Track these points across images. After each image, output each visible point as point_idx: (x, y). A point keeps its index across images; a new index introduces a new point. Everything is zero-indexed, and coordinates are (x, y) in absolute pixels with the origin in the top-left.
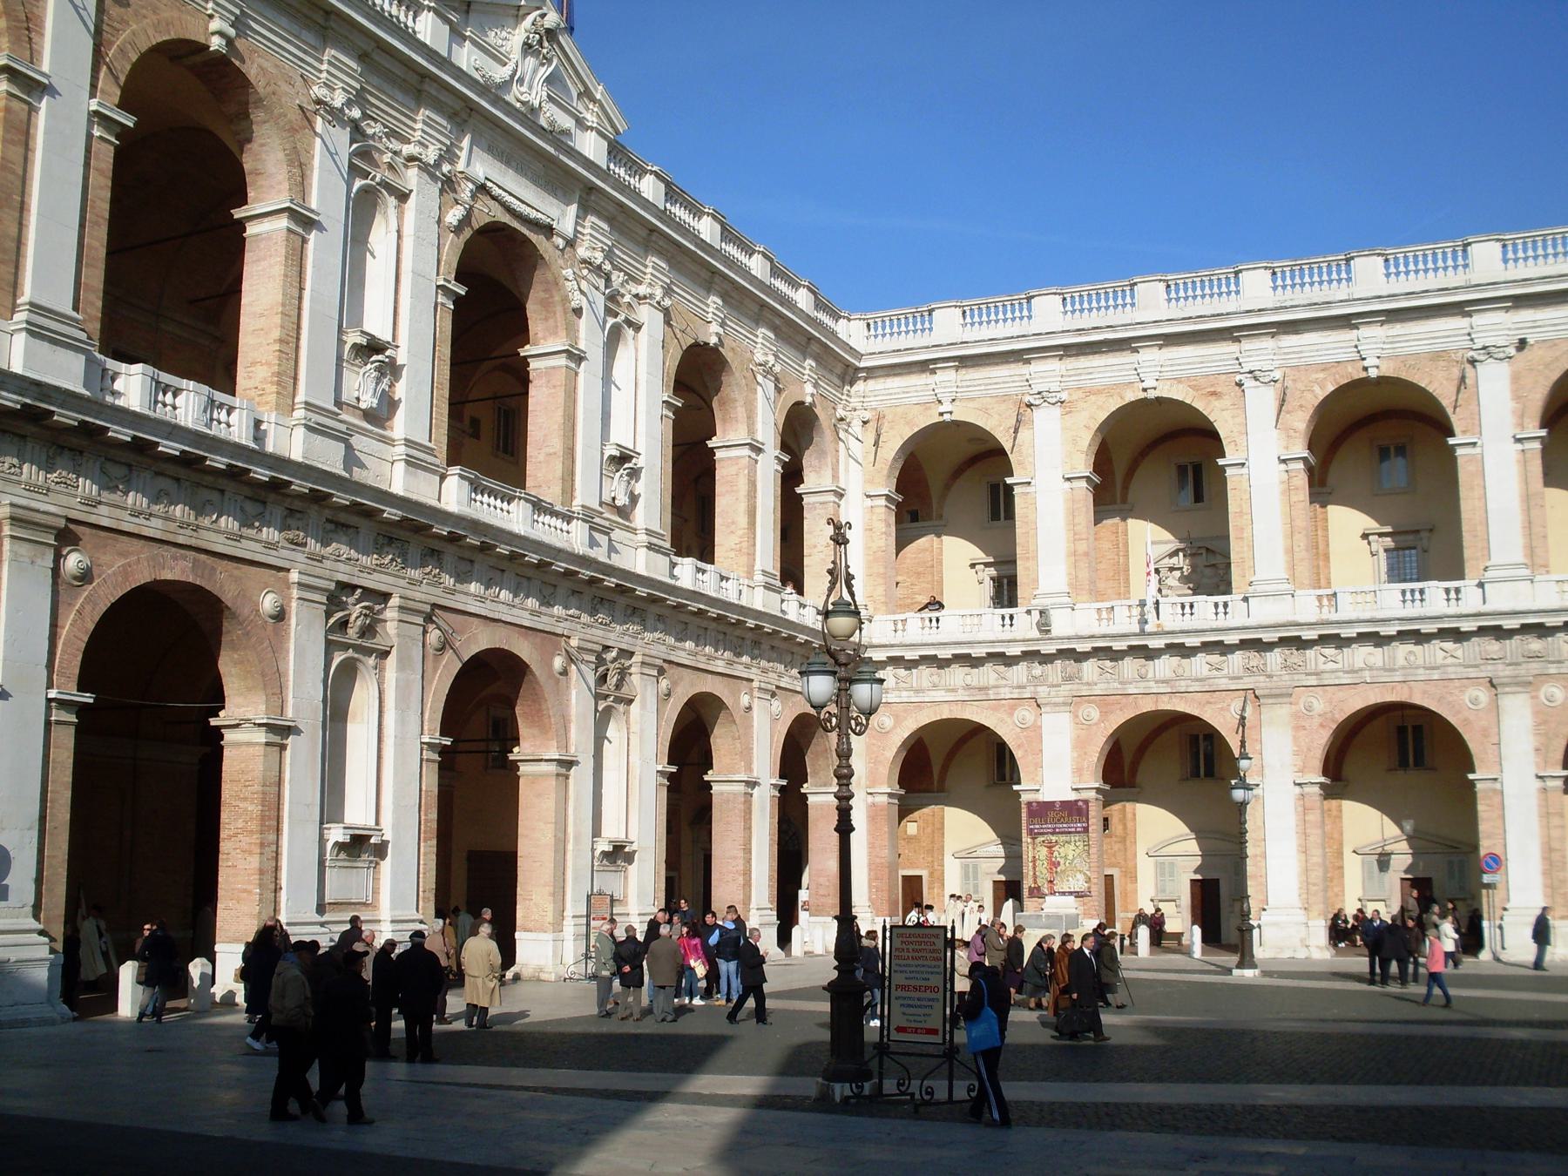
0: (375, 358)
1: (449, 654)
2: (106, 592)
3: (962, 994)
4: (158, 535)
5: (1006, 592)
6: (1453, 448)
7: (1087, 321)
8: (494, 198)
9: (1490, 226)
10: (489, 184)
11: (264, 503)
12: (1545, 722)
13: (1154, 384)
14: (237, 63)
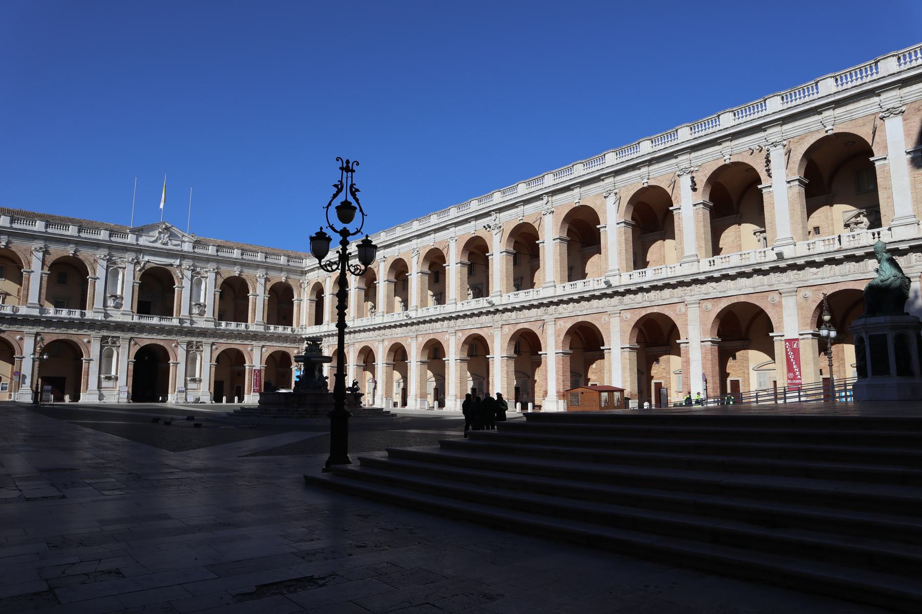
2: (138, 348)
5: (406, 307)
6: (761, 190)
7: (624, 159)
9: (680, 122)
12: (802, 309)
13: (831, 127)
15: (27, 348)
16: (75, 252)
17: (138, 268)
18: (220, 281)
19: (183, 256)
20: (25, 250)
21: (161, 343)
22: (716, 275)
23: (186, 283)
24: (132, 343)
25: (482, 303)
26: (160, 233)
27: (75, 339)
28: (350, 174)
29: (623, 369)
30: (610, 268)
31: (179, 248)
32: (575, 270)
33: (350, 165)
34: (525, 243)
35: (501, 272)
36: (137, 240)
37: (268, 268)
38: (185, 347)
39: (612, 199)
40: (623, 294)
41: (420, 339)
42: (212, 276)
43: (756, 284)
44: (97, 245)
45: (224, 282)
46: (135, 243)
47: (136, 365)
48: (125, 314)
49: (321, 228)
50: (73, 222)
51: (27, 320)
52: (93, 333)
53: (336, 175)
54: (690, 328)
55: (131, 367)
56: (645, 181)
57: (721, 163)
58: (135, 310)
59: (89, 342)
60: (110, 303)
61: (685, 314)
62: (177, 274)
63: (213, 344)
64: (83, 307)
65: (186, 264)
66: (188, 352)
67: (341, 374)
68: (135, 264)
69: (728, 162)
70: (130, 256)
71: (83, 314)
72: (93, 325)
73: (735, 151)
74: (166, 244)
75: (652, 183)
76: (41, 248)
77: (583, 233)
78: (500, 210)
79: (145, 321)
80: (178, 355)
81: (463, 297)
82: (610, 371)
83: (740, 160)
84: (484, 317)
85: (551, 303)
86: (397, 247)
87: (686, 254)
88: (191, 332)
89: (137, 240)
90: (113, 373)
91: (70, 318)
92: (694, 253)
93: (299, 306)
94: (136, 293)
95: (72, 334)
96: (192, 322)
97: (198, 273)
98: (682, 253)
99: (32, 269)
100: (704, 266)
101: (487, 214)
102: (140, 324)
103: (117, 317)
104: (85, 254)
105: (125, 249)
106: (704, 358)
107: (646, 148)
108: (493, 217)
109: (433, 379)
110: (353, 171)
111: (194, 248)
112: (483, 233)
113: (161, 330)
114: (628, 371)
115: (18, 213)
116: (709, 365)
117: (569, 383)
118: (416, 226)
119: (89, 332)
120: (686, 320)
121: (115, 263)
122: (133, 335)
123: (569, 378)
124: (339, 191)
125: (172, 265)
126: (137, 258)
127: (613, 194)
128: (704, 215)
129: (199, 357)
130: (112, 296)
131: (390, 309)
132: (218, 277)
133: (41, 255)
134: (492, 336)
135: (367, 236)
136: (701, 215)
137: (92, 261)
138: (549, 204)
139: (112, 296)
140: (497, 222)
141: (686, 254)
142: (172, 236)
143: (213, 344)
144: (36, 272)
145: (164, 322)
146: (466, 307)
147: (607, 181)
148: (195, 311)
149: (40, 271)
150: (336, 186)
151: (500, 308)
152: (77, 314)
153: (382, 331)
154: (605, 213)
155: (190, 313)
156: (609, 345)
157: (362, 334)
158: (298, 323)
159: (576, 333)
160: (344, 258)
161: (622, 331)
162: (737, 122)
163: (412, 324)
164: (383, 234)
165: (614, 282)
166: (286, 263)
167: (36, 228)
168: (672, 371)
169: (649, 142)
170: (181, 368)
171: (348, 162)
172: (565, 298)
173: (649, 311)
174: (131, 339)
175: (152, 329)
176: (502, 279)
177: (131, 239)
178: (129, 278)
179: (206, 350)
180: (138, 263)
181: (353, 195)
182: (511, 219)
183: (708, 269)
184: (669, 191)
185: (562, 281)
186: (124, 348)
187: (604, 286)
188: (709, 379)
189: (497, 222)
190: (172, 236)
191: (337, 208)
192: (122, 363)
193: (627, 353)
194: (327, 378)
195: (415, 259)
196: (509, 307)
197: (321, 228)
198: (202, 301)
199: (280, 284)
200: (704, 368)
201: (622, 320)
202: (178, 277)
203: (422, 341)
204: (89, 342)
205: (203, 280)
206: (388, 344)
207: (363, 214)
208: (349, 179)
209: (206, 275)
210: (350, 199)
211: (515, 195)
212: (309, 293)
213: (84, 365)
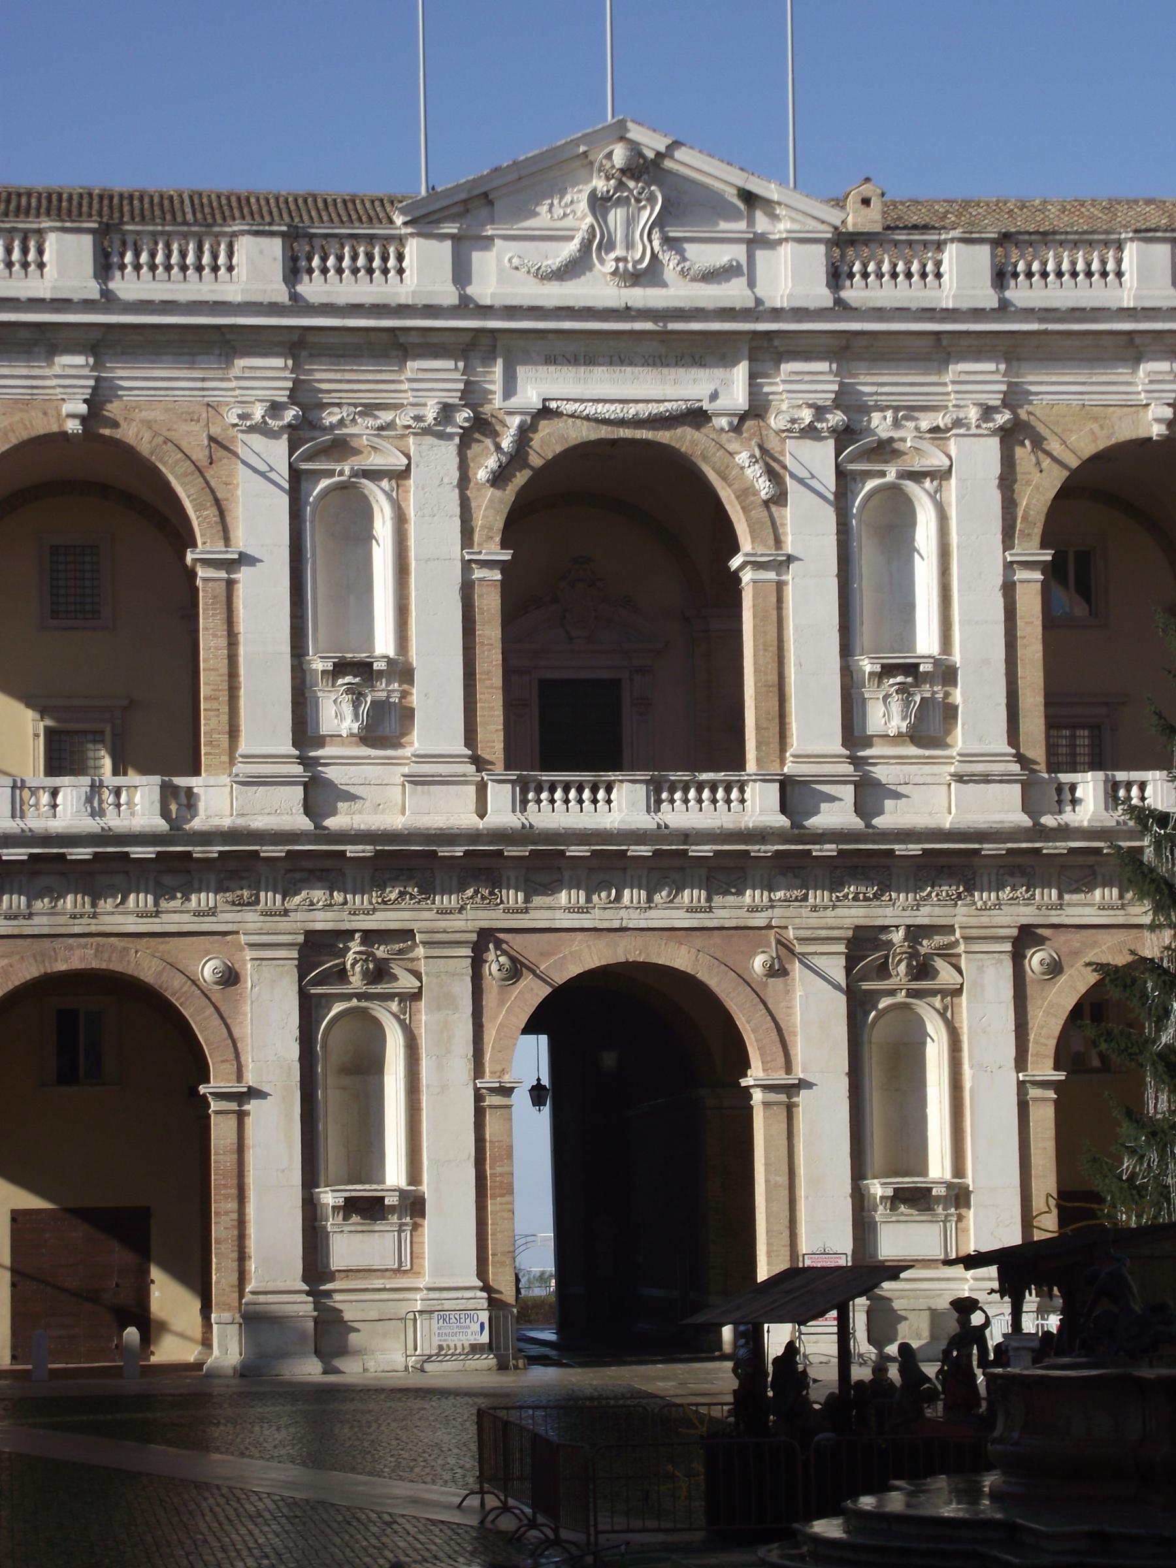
0: (340, 682)
1: (527, 980)
2: (1076, 983)
3: (860, 1383)
4: (46, 931)
8: (572, 416)
10: (553, 405)
11: (189, 872)
14: (107, 432)
16: (96, 402)
17: (486, 466)
18: (1040, 487)
19: (764, 345)
21: (679, 958)
23: (809, 529)
24: (494, 964)
26: (599, 204)
27: (145, 966)
31: (734, 293)
36: (461, 273)
37: (1013, 350)
38: (836, 968)
42: (977, 458)
44: (213, 341)
45: (1065, 494)
46: (448, 295)
50: (63, 207)
52: (251, 918)
58: (493, 741)
59: (230, 978)
60: (337, 715)
62: (736, 473)
63: (1026, 938)
65: (799, 388)
66: (858, 1005)
68: (466, 440)
70: (427, 385)
71: (177, 802)
72: (241, 865)
79: (556, 814)
80: (802, 1031)
88: (867, 863)
89: (461, 273)
91: (661, 834)
95: (120, 928)
96: (869, 794)
97: (885, 450)
99: (789, 548)
102: (525, 835)
103: (385, 799)
104: (156, 405)
105: (391, 342)
111: (837, 276)
113: (668, 864)
115: (326, 206)
119: (227, 918)
121: (341, 447)
122: (493, 918)
125: (697, 417)
126: (472, 395)
130: (341, 668)
132: (1023, 453)
137: (200, 456)
139: (341, 668)
142: (684, 206)
148: (885, 715)
152: (139, 806)
155: (853, 733)
170: (825, 1117)
174: (485, 939)
175: (607, 865)
177: (421, 272)
178: (981, 556)
179: (984, 994)
180: (483, 426)
186: (446, 1002)
190: (684, 206)
202: (745, 493)
204: (230, 978)
205: (920, 494)
209: (937, 460)
213: (221, 1132)
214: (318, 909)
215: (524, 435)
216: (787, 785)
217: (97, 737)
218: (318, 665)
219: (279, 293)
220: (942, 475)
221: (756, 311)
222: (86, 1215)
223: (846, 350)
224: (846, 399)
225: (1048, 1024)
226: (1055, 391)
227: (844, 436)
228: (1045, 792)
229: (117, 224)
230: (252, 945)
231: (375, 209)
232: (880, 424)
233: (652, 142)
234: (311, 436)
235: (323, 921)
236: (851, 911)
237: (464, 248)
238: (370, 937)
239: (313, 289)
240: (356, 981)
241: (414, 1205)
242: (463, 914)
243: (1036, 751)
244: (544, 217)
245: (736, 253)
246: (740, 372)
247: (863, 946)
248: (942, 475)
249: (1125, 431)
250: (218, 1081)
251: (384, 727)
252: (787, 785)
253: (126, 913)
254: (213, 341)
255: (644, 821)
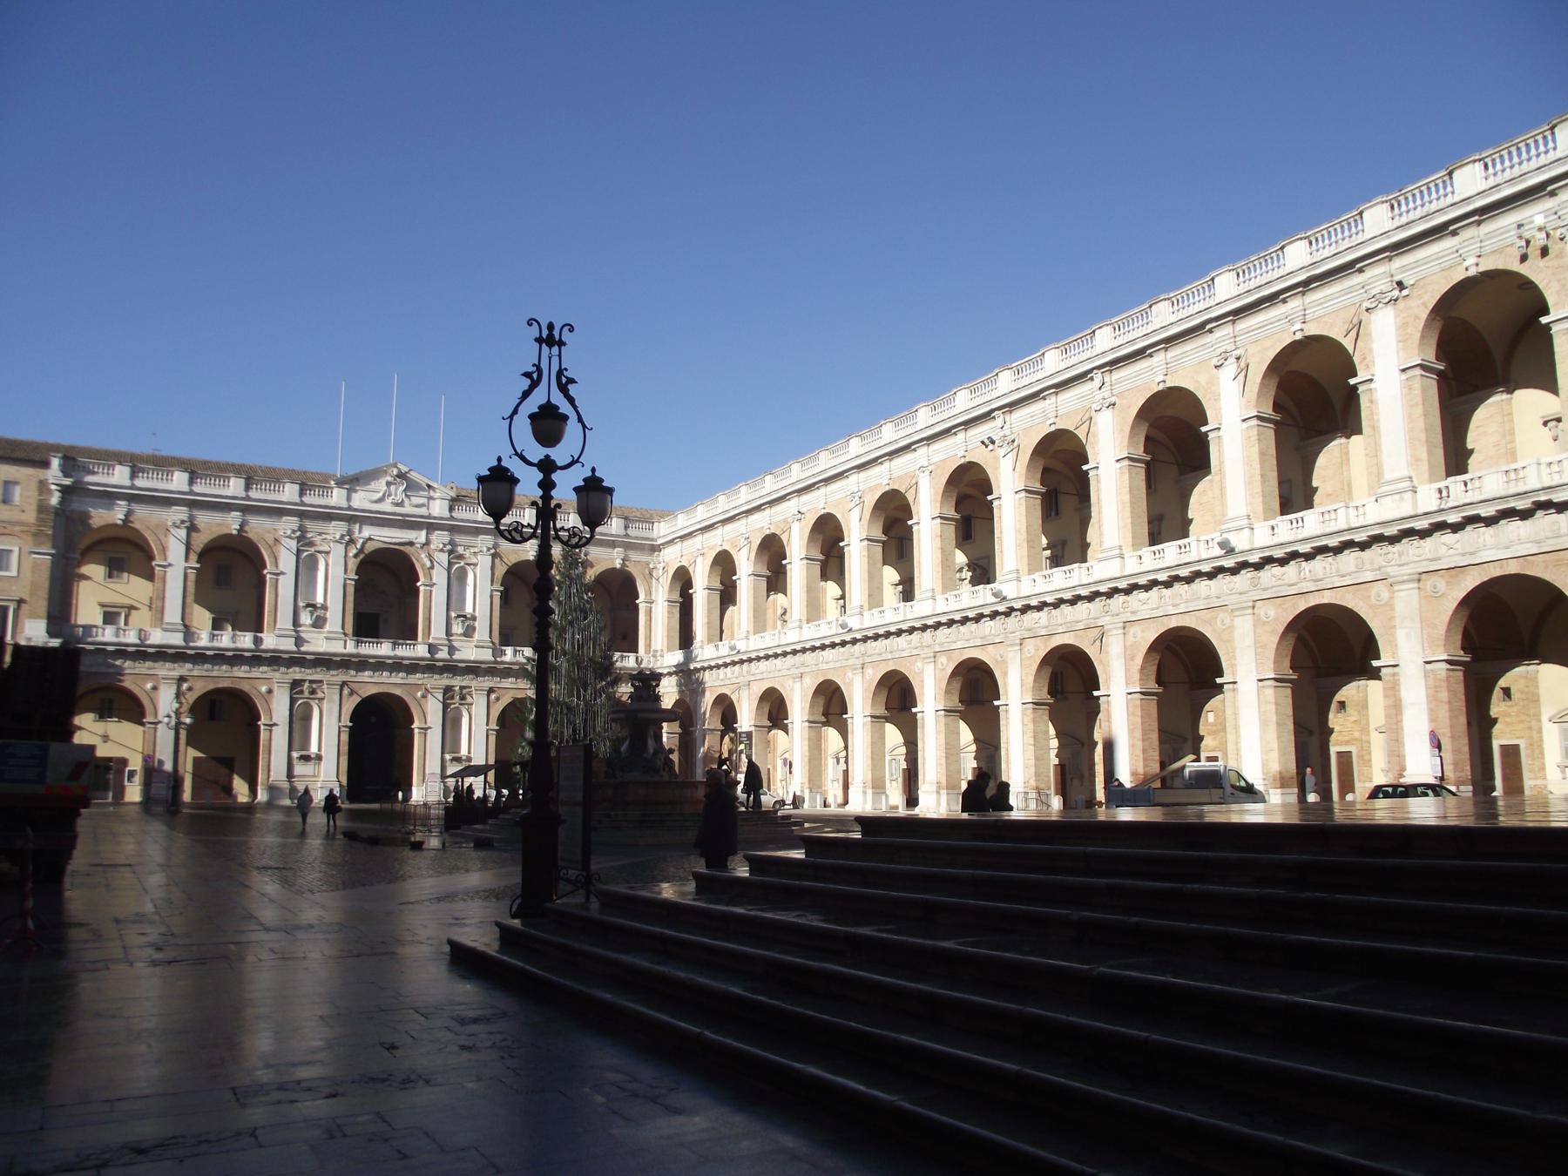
2: (356, 700)
15: (165, 702)
18: (501, 570)
20: (158, 526)
21: (398, 692)
22: (1453, 518)
23: (440, 577)
24: (346, 691)
25: (983, 596)
26: (388, 484)
27: (245, 687)
28: (555, 349)
29: (1263, 723)
30: (1231, 514)
31: (423, 511)
32: (1165, 519)
33: (556, 333)
34: (1062, 473)
35: (1018, 531)
36: (349, 499)
37: (192, 504)
39: (1231, 368)
40: (1258, 566)
41: (869, 671)
42: (485, 561)
43: (1542, 535)
44: (278, 512)
47: (353, 733)
48: (331, 638)
49: (499, 459)
51: (161, 654)
52: (277, 675)
53: (527, 354)
54: (1401, 634)
55: (345, 737)
56: (1298, 326)
57: (1458, 276)
59: (270, 691)
60: (306, 618)
61: (1390, 605)
62: (421, 560)
63: (491, 691)
64: (258, 627)
65: (439, 538)
66: (445, 706)
67: (688, 742)
68: (347, 544)
69: (1472, 272)
70: (337, 529)
71: (258, 641)
72: (276, 660)
73: (1489, 246)
74: (401, 504)
75: (1313, 330)
76: (183, 522)
77: (1174, 443)
78: (1013, 406)
80: (429, 716)
81: (948, 585)
82: (1236, 728)
83: (1501, 267)
84: (987, 624)
85: (1115, 591)
86: (823, 490)
87: (1388, 476)
88: (451, 668)
89: (349, 499)
90: (314, 749)
92: (1405, 473)
93: (649, 612)
94: (351, 598)
96: (452, 650)
97: (461, 557)
98: (1380, 474)
100: (1428, 497)
101: (987, 416)
102: (357, 655)
103: (318, 643)
104: (259, 528)
105: (328, 516)
106: (1432, 698)
107: (1298, 256)
108: (999, 422)
109: (974, 747)
110: (561, 344)
111: (451, 509)
112: (979, 456)
113: (397, 666)
114: (1273, 728)
116: (1444, 713)
117: (1156, 755)
118: (856, 448)
120: (1392, 618)
121: (311, 544)
122: (345, 678)
123: (1156, 743)
124: (535, 384)
125: (411, 544)
126: (350, 532)
127: (1232, 360)
128: (1424, 390)
129: (465, 714)
131: (814, 611)
133: (183, 533)
134: (1004, 662)
135: (593, 470)
136: (1417, 391)
137: (271, 542)
138: (1106, 388)
139: (308, 605)
140: (1006, 432)
141: (1388, 476)
142: (412, 487)
143: (491, 691)
144: (176, 563)
145: (402, 652)
146: (954, 605)
147: (1218, 334)
148: (457, 628)
149: (183, 564)
150: (527, 375)
151: (1017, 605)
152: (246, 641)
153: (799, 658)
154: (1217, 400)
155: (448, 633)
156: (1234, 674)
157: (763, 664)
158: (648, 646)
159: (1168, 648)
160: (546, 512)
161: (1259, 646)
162: (1491, 182)
163: (854, 641)
164: (795, 467)
165: (1240, 541)
166: (622, 532)
167: (173, 486)
168: (1372, 726)
169: (1305, 243)
170: (435, 737)
171: (551, 327)
172: (1142, 581)
173: (1313, 601)
174: (344, 684)
175: (379, 665)
176: (1018, 546)
177: (337, 497)
178: (337, 572)
179: (479, 704)
180: (352, 541)
181: (563, 389)
182: (1032, 424)
183: (1433, 505)
184: (1348, 344)
185: (1136, 546)
186: (331, 701)
187: (1218, 552)
188: (1446, 743)
189: (1006, 432)
190: (412, 487)
191: (532, 417)
192: (328, 732)
193: (1270, 692)
194: (671, 751)
195: (856, 513)
196: (1034, 602)
197: (499, 459)
198: (469, 609)
199: (612, 572)
200: (1432, 720)
201: (1258, 623)
202: (423, 566)
203: (874, 675)
204: (270, 691)
206: (811, 684)
207: (584, 427)
208: (555, 360)
209: (474, 561)
210: (558, 399)
211: (1040, 376)
212: (667, 588)
213: (263, 735)
214: (296, 673)
215: (364, 544)
216: (430, 646)
217: (227, 621)
218: (301, 604)
219: (297, 500)
220: (475, 565)
221: (429, 517)
222: (214, 758)
223: (453, 529)
224: (452, 543)
225: (495, 713)
226: (204, 518)
227: (450, 552)
228: (497, 652)
229: (195, 470)
230: (686, 639)
231: (326, 478)
232: (460, 550)
233: (404, 469)
234: (303, 539)
235: (298, 677)
236: (445, 681)
237: (350, 491)
238: (311, 682)
239: (306, 499)
240: (306, 694)
241: (319, 758)
242: (338, 676)
243: (497, 641)
244: (373, 485)
245: (424, 501)
246: (424, 533)
247: (448, 690)
248: (475, 565)
249: (524, 558)
250: (263, 720)
251: (319, 623)
252: (430, 646)
253: (241, 671)
254: (278, 512)
255: (391, 653)
